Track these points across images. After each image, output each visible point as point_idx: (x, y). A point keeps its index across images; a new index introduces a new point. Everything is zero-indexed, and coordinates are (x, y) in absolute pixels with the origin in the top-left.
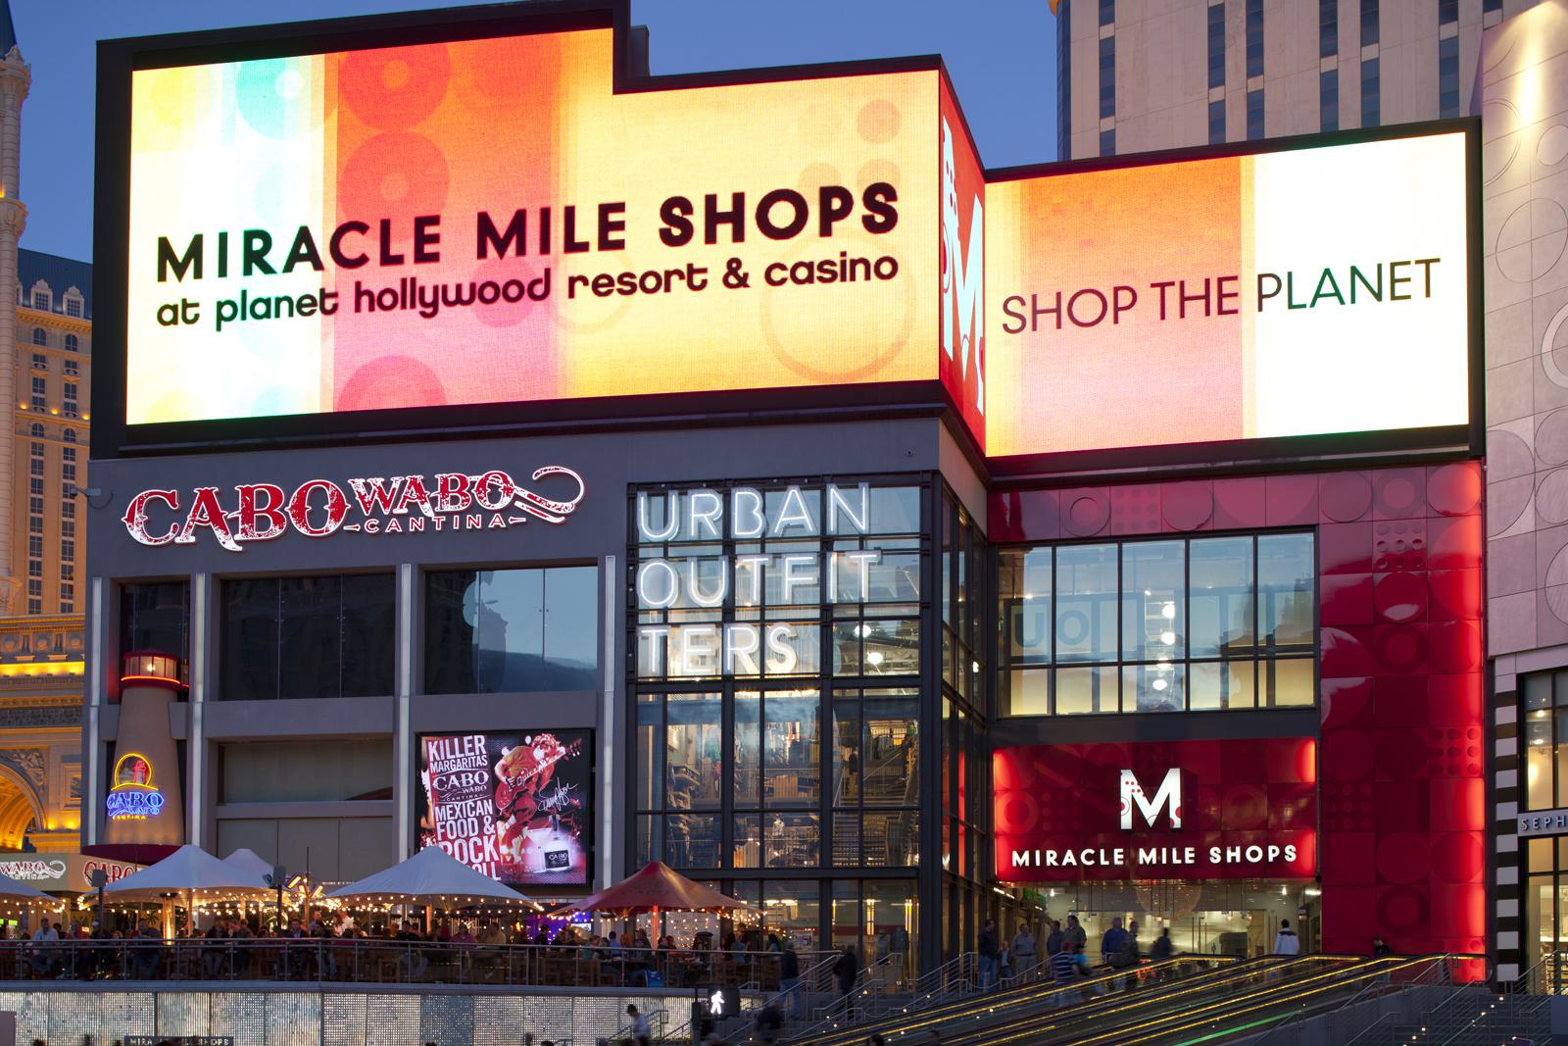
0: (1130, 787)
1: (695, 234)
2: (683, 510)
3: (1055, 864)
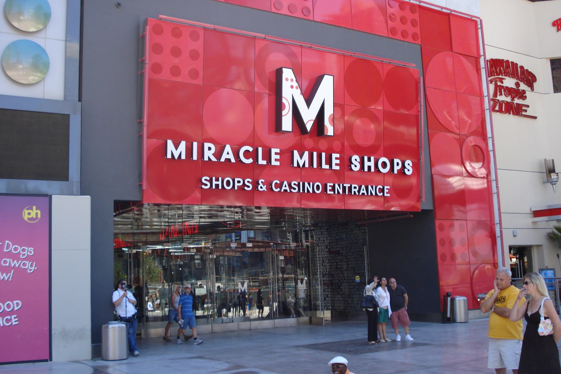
0: (290, 83)
2: (243, 35)
3: (214, 159)
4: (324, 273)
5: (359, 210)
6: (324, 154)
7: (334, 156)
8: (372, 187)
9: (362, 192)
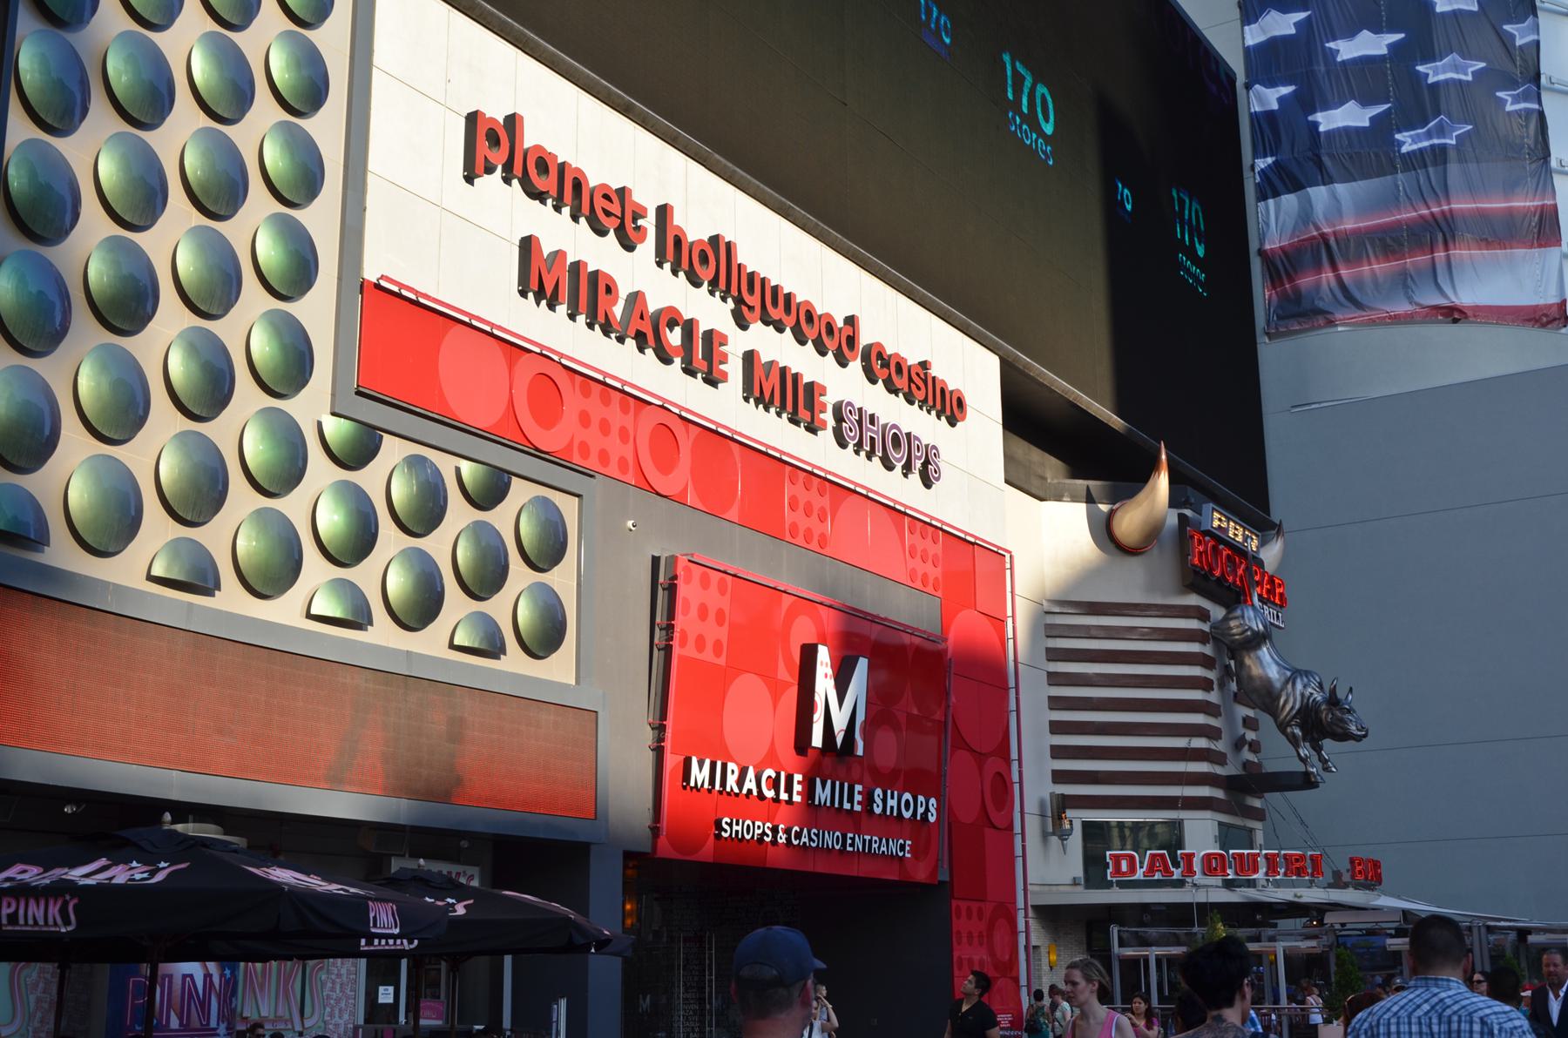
1: (688, 643)
3: (736, 790)
4: (688, 984)
5: (175, 801)
6: (846, 785)
7: (858, 788)
8: (893, 841)
9: (882, 849)
